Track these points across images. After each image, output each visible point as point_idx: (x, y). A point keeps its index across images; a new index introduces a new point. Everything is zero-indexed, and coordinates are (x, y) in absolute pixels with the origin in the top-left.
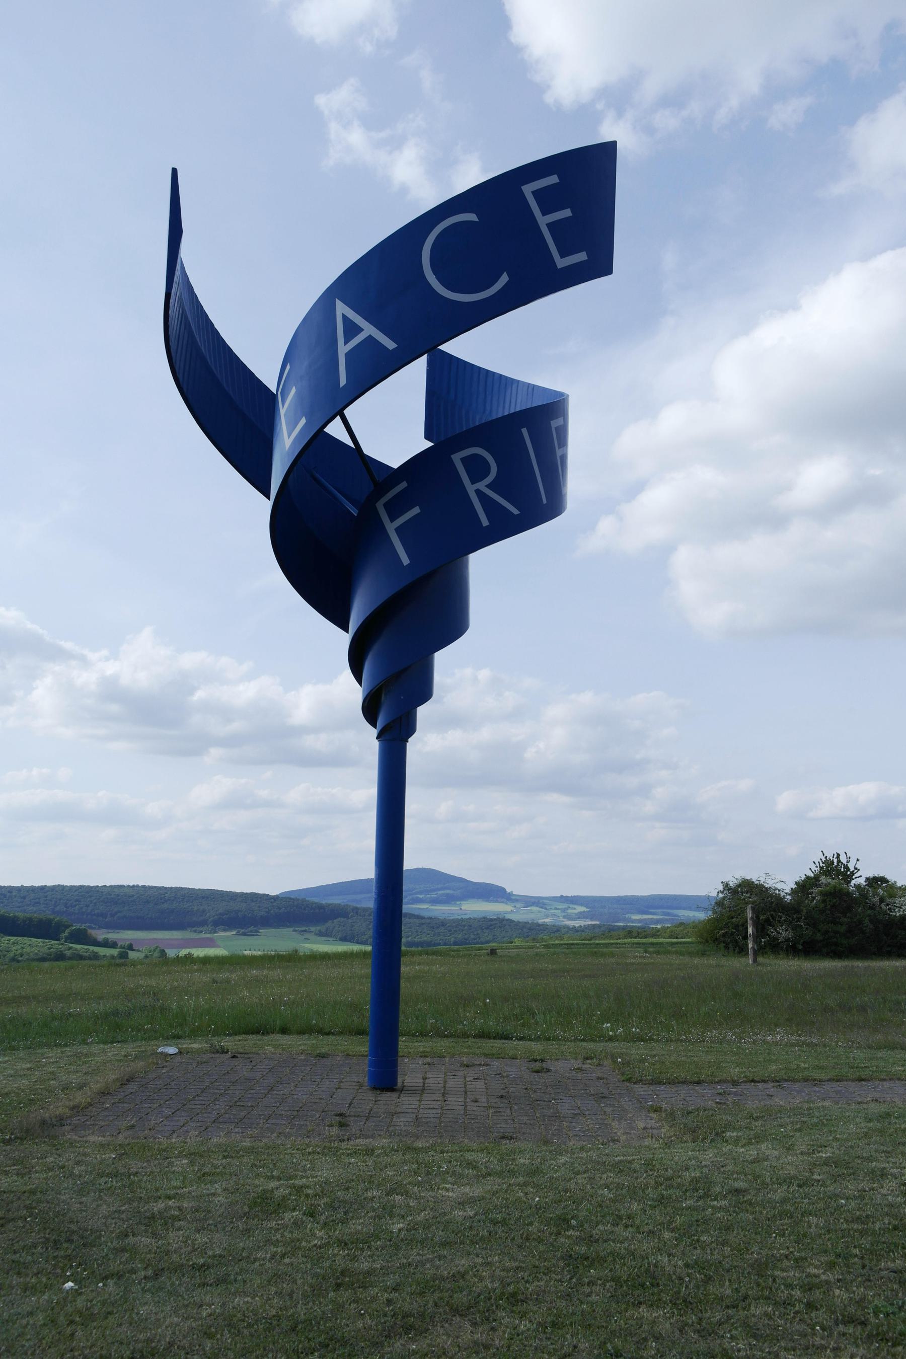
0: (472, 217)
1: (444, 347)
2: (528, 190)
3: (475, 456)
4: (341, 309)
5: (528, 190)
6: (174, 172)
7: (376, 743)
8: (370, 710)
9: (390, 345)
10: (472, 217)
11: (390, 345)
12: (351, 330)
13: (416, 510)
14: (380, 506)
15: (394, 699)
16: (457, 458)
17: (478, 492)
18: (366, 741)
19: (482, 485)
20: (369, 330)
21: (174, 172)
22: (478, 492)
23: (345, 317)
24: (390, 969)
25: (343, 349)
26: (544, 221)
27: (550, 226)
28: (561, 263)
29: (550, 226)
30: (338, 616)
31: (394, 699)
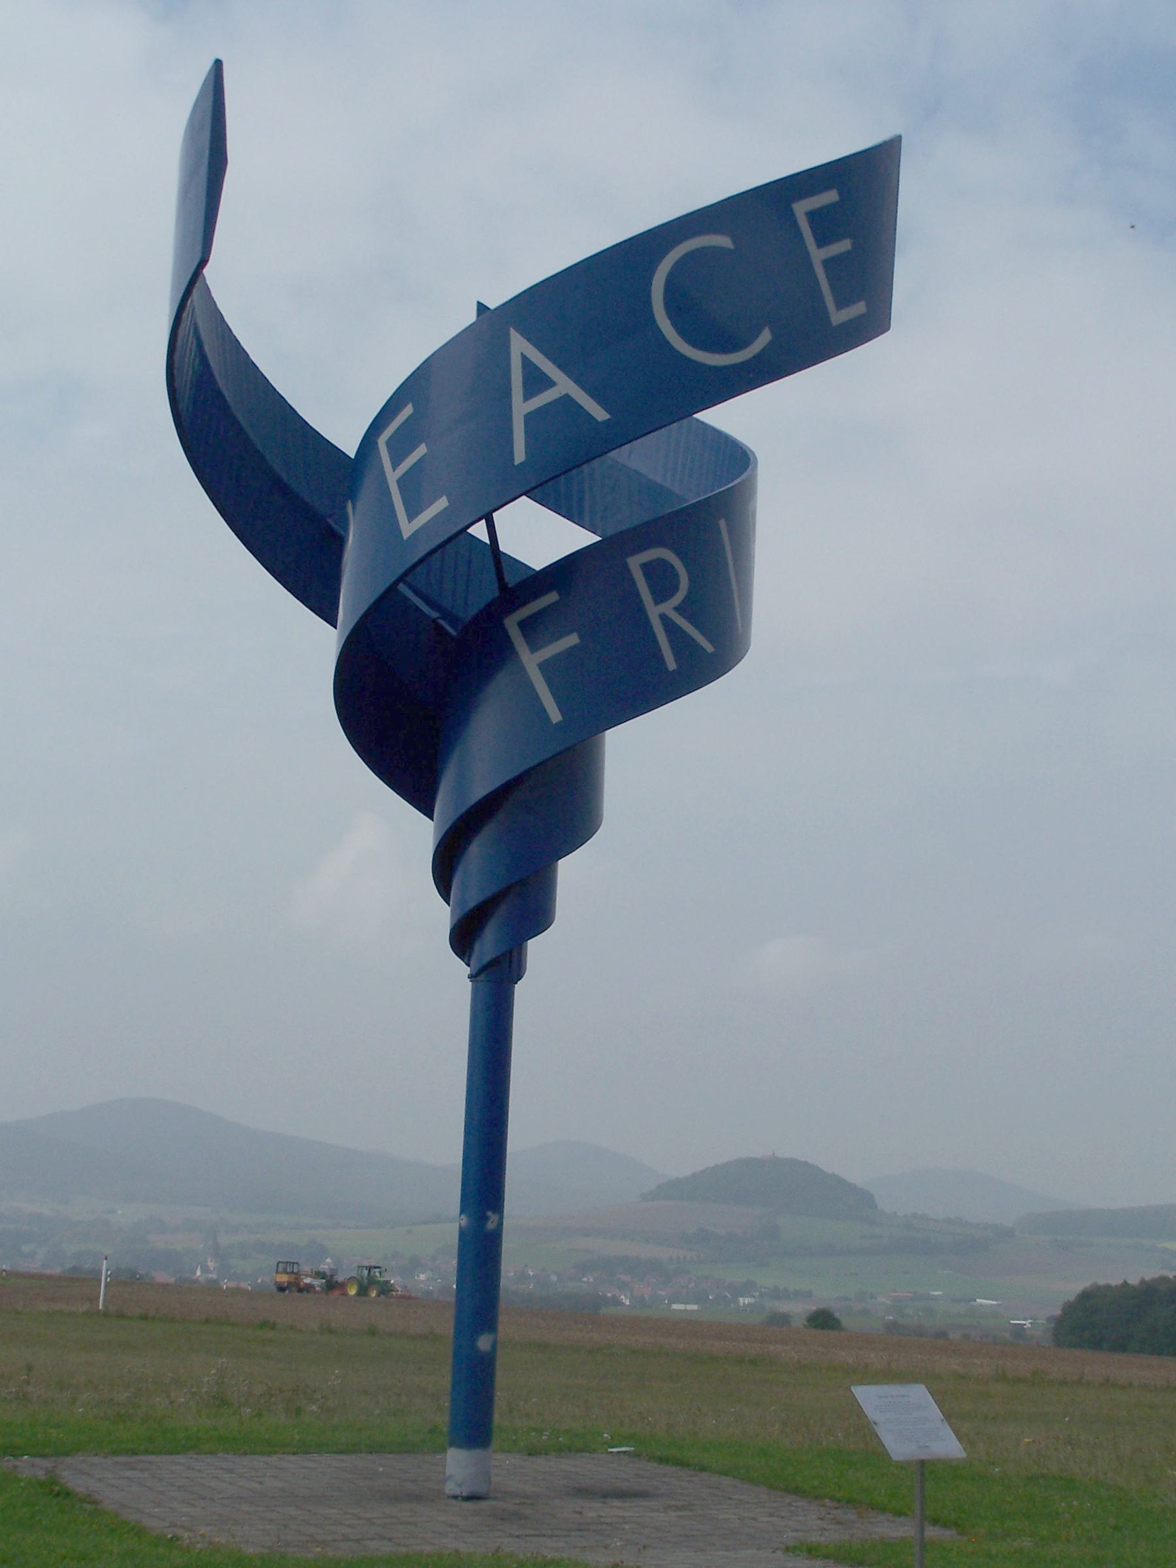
0: (723, 241)
1: (513, 332)
2: (801, 208)
3: (663, 564)
4: (519, 345)
5: (801, 208)
6: (218, 64)
7: (468, 985)
8: (463, 939)
9: (600, 414)
10: (723, 241)
11: (600, 414)
12: (536, 381)
13: (572, 640)
14: (511, 624)
15: (497, 921)
16: (635, 563)
17: (664, 618)
18: (455, 981)
19: (668, 608)
20: (564, 385)
21: (218, 64)
22: (664, 618)
23: (526, 362)
24: (476, 1338)
25: (521, 408)
26: (818, 255)
27: (827, 263)
28: (838, 317)
29: (827, 263)
30: (417, 788)
31: (497, 921)
